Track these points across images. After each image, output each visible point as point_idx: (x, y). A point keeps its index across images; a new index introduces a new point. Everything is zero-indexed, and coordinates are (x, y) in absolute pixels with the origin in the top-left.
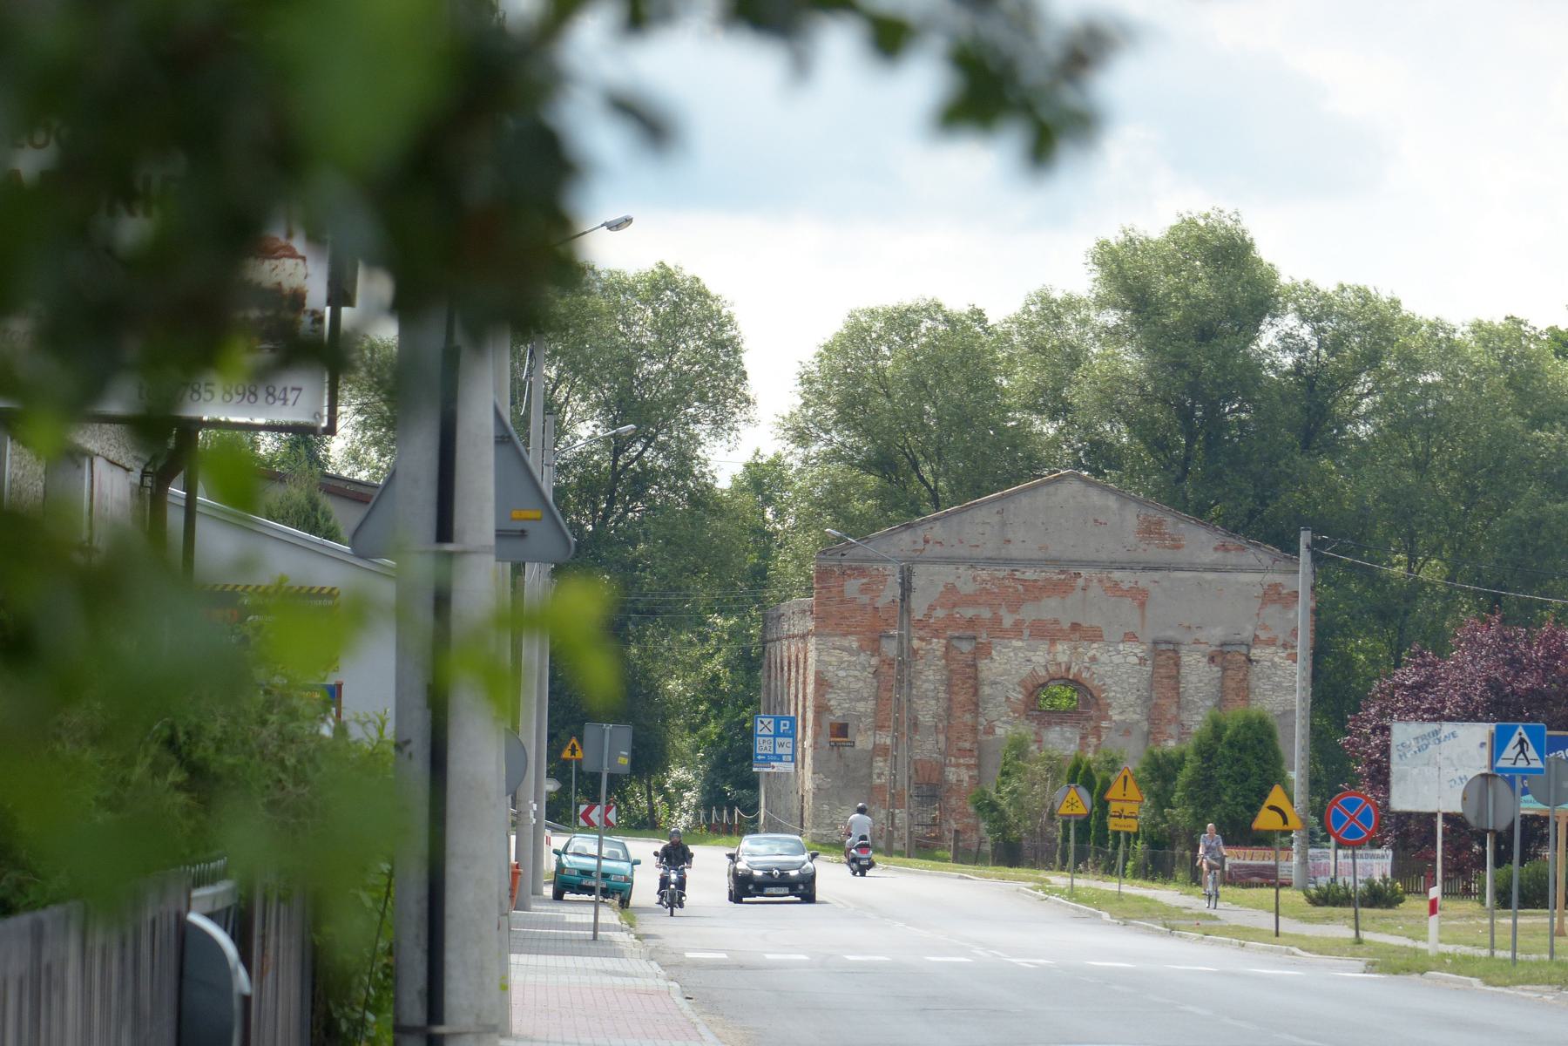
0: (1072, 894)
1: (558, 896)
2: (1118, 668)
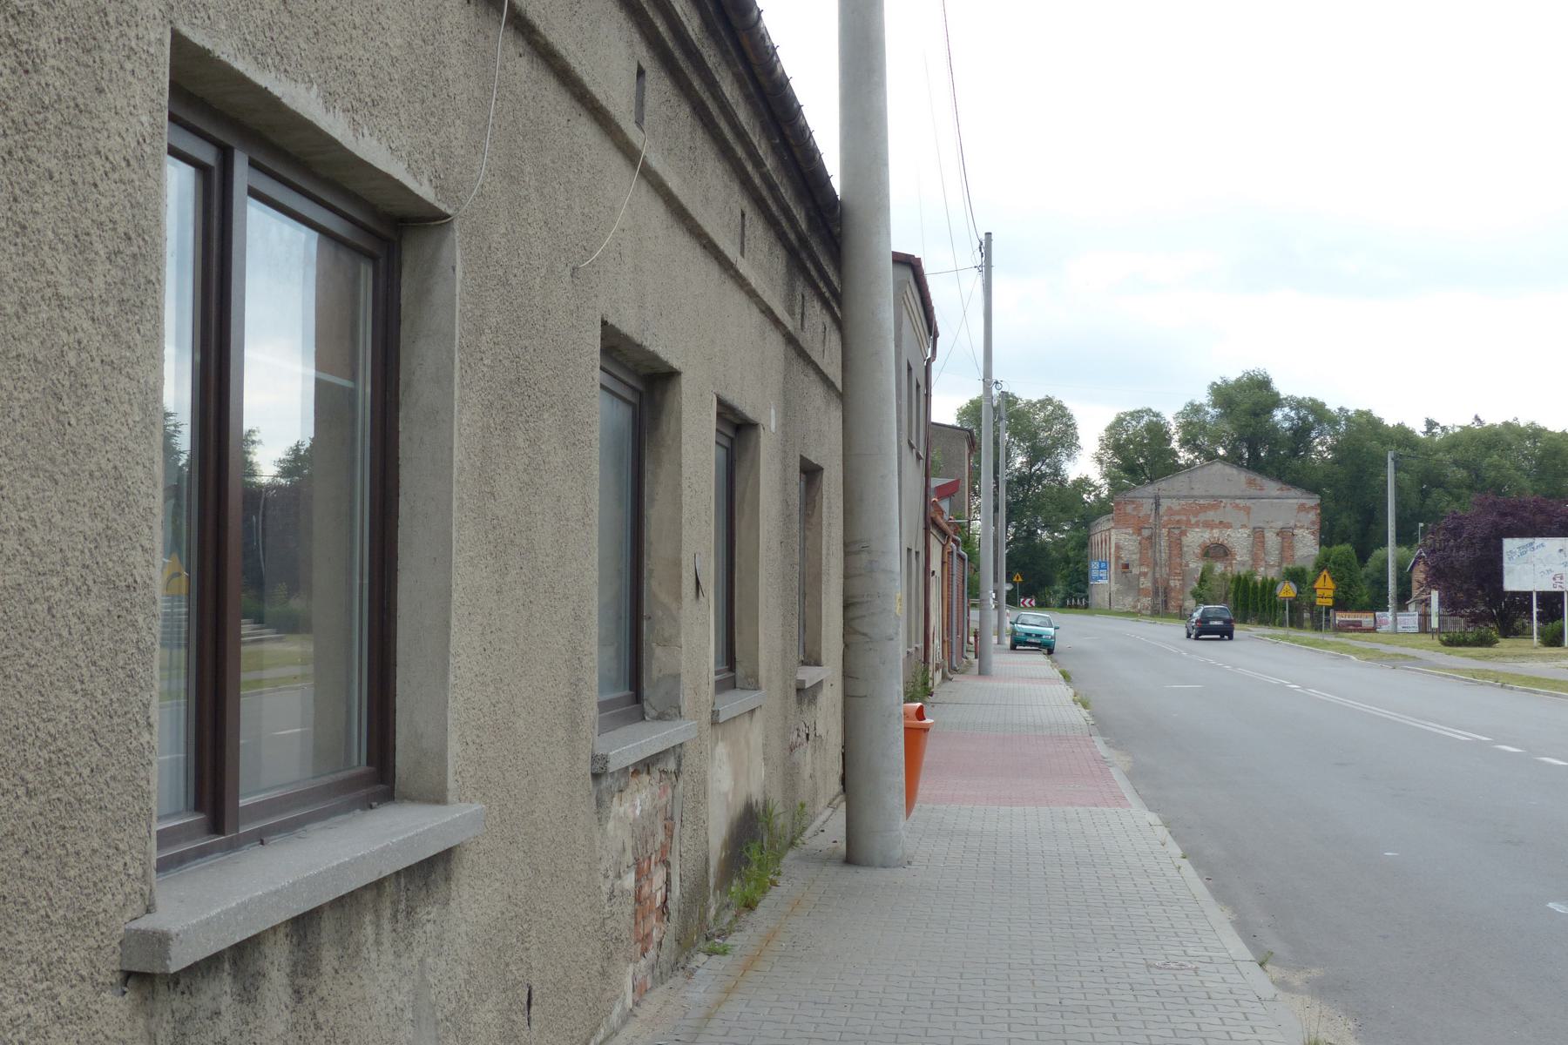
0: (1272, 637)
1: (1013, 647)
2: (1238, 539)
